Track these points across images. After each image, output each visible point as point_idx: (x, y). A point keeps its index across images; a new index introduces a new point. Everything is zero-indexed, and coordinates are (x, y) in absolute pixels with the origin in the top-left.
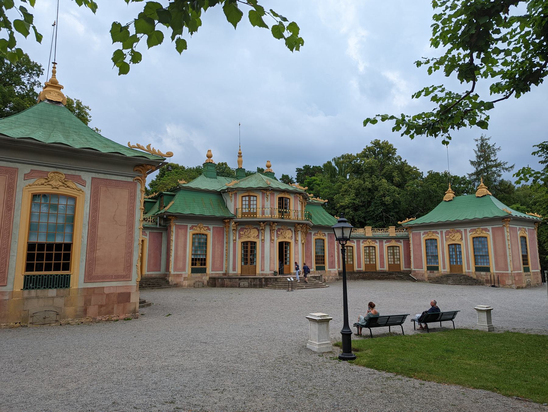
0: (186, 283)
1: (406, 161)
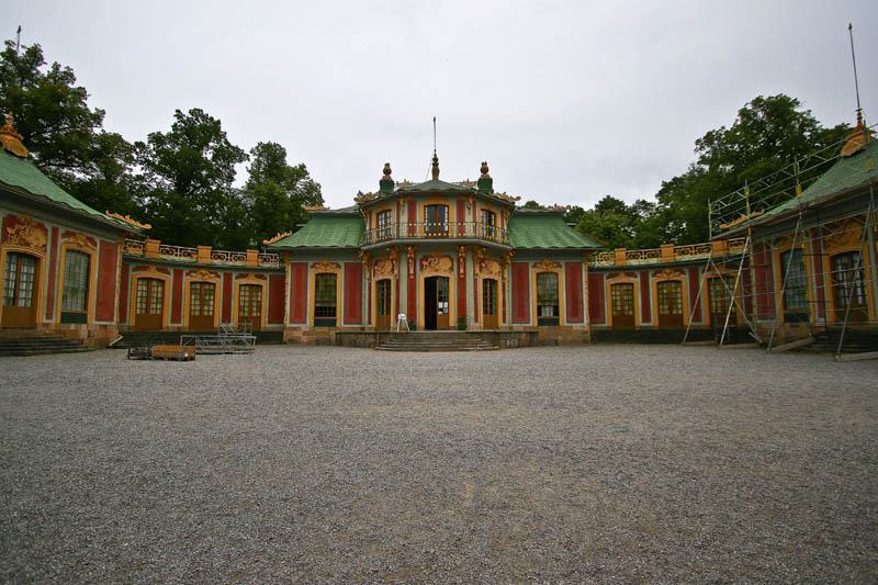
0: (304, 339)
1: (179, 114)
